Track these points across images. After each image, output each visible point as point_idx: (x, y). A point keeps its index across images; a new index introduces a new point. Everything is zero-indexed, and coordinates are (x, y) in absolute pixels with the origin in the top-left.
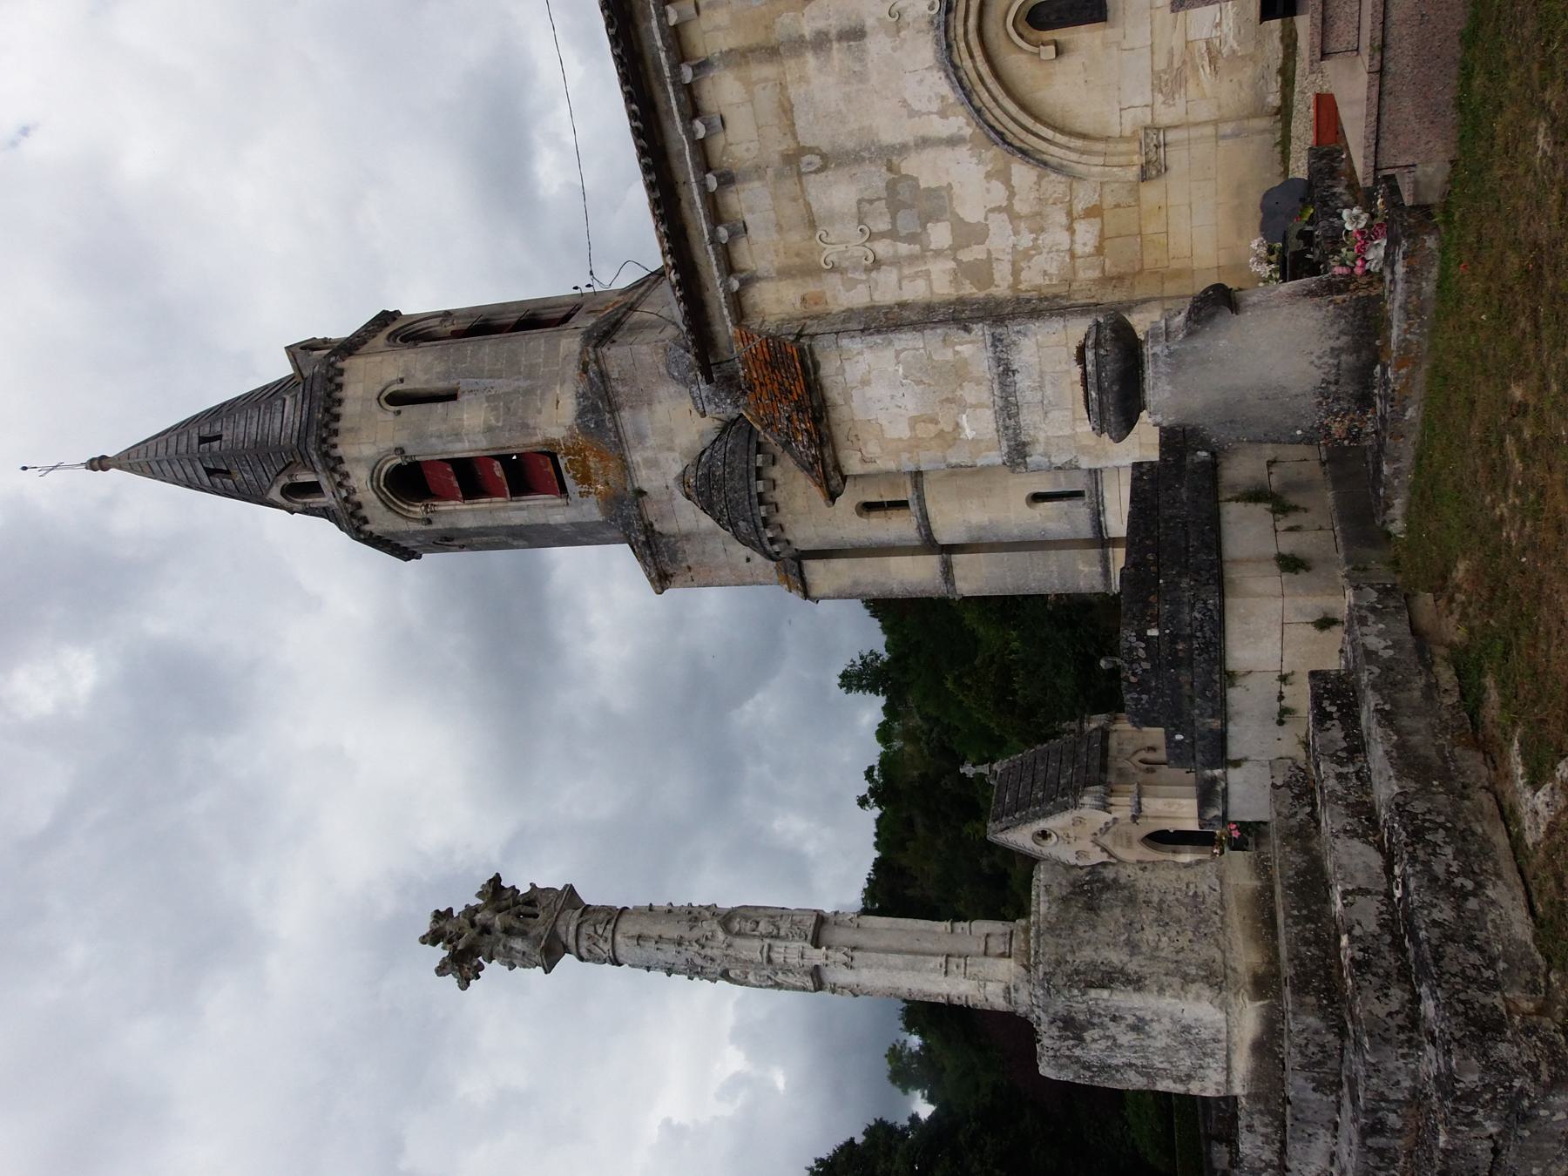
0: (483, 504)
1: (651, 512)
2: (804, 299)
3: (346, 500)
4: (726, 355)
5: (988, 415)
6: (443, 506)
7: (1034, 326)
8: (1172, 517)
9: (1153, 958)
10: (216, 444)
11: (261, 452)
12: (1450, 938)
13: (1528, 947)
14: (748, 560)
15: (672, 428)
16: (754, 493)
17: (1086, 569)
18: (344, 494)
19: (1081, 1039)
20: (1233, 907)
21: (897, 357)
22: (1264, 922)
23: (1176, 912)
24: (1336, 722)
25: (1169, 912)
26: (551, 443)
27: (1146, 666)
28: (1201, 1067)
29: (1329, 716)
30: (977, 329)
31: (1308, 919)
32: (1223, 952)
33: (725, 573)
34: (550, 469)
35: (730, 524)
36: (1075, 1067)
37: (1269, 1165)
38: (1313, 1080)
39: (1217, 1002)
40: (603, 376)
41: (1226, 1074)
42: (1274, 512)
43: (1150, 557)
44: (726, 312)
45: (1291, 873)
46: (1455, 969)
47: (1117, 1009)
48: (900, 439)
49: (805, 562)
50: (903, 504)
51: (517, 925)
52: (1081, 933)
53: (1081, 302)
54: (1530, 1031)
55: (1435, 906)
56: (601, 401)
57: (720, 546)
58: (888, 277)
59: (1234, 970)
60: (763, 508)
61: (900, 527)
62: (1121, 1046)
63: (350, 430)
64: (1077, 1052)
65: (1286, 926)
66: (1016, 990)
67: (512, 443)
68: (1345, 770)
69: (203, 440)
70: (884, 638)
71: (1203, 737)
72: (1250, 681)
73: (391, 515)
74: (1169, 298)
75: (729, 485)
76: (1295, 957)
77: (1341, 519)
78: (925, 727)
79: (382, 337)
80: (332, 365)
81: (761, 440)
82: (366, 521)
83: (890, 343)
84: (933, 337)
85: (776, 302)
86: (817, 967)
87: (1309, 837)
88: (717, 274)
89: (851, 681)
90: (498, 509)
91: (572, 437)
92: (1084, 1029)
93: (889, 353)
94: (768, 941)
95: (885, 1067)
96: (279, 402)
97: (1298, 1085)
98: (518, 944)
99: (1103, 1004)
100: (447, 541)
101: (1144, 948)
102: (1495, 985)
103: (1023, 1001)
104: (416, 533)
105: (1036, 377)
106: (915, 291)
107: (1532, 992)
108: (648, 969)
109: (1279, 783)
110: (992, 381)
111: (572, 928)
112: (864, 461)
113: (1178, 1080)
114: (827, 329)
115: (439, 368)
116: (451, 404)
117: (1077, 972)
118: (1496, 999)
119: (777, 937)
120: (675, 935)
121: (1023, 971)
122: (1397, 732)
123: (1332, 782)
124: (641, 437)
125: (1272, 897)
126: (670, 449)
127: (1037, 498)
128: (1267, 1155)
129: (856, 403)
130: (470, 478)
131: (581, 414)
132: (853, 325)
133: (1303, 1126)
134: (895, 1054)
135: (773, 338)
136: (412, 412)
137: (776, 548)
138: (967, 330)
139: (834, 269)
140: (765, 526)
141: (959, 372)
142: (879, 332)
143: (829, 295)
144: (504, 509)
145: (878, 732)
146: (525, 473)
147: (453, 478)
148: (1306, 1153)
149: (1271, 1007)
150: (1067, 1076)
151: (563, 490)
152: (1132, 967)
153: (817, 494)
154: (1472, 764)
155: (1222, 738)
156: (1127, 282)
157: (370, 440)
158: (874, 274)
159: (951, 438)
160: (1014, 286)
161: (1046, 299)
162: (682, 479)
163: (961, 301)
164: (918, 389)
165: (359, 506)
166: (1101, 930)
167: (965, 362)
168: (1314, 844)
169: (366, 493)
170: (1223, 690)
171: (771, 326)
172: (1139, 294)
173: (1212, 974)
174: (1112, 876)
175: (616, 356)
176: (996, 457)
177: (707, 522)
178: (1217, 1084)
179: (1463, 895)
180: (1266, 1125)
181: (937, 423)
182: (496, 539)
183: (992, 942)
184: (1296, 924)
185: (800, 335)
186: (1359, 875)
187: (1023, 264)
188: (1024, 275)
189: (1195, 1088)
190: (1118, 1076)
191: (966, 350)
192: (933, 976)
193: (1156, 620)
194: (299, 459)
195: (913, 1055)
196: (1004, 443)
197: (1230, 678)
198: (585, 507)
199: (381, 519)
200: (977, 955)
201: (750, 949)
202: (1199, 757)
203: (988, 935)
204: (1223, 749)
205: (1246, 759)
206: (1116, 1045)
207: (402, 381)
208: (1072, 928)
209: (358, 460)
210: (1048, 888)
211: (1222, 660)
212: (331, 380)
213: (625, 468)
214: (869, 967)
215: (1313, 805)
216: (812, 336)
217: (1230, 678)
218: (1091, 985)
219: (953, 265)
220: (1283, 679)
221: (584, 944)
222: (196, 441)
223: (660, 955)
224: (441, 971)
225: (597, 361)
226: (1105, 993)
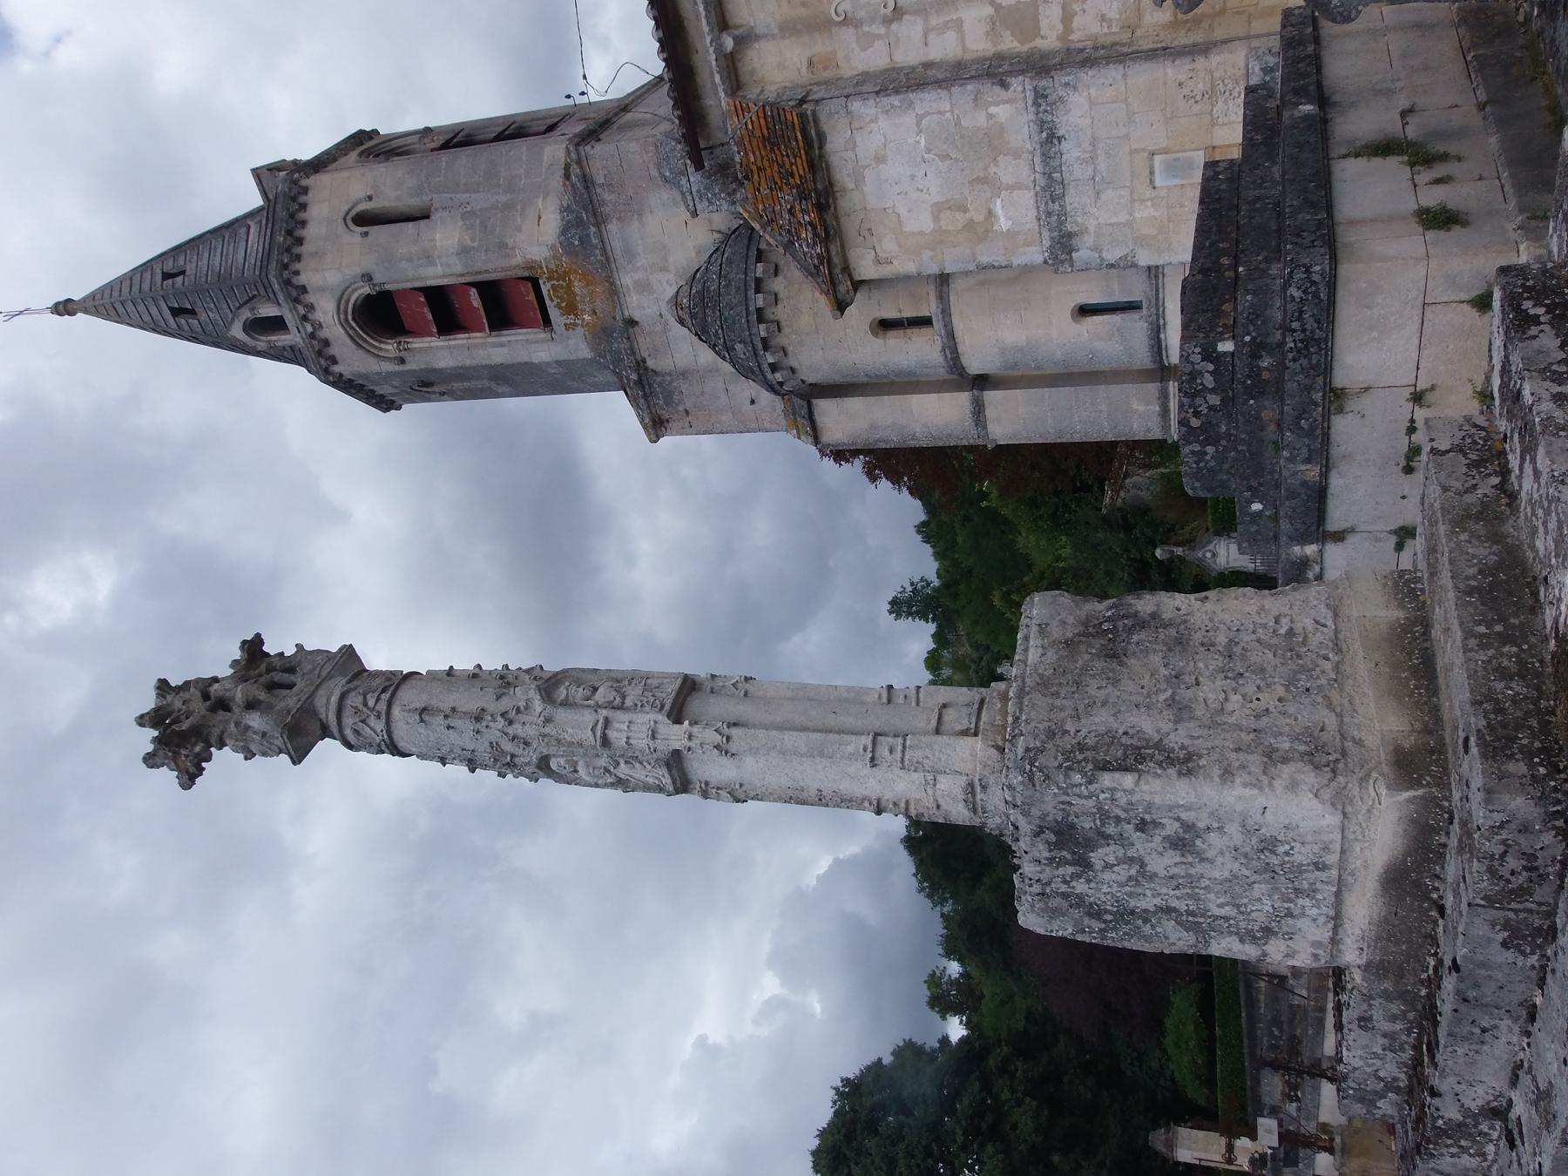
0: (460, 340)
1: (644, 346)
2: (810, 63)
3: (312, 336)
4: (720, 137)
5: (1026, 198)
6: (417, 343)
7: (1087, 76)
8: (1258, 199)
9: (1213, 725)
10: (179, 279)
11: (224, 286)
14: (753, 402)
15: (667, 238)
16: (752, 308)
17: (1141, 408)
18: (310, 329)
19: (1084, 864)
20: (1356, 648)
21: (918, 124)
22: (1414, 671)
23: (1255, 658)
24: (1547, 328)
25: (1243, 658)
26: (530, 265)
27: (1214, 400)
28: (1290, 914)
29: (1535, 320)
30: (1016, 83)
31: (1505, 639)
32: (1340, 716)
33: (726, 418)
34: (532, 297)
35: (724, 350)
36: (1076, 913)
37: (1391, 1086)
38: (1506, 926)
39: (1327, 794)
40: (587, 180)
41: (1325, 930)
42: (1412, 165)
43: (1225, 261)
44: (717, 78)
47: (1149, 807)
48: (921, 233)
49: (815, 401)
50: (925, 322)
51: (262, 696)
52: (1092, 690)
53: (1145, 47)
56: (587, 212)
57: (721, 385)
58: (911, 29)
59: (1359, 743)
60: (762, 327)
61: (919, 351)
62: (1153, 877)
63: (314, 255)
64: (1080, 887)
66: (984, 788)
67: (490, 266)
69: (167, 276)
70: (936, 565)
71: (1292, 495)
72: (1364, 403)
73: (361, 353)
74: (1258, 36)
75: (726, 307)
76: (1483, 699)
77: (1511, 163)
78: (975, 655)
79: (353, 155)
80: (295, 182)
81: (763, 246)
82: (334, 361)
83: (911, 105)
84: (962, 95)
85: (777, 66)
86: (676, 754)
87: (1501, 519)
88: (706, 29)
89: (899, 607)
90: (476, 346)
91: (554, 257)
92: (1090, 845)
93: (909, 120)
94: (604, 712)
95: (924, 993)
96: (243, 230)
97: (1470, 934)
98: (255, 720)
99: (1123, 799)
100: (427, 386)
101: (1200, 711)
103: (996, 809)
104: (391, 375)
105: (1086, 145)
106: (944, 48)
108: (443, 761)
109: (1443, 447)
110: (1033, 153)
111: (334, 700)
112: (878, 261)
113: (1248, 936)
114: (837, 93)
115: (411, 182)
116: (423, 223)
117: (1082, 747)
119: (621, 707)
120: (473, 706)
121: (994, 753)
123: (1547, 406)
124: (631, 255)
126: (664, 269)
127: (1085, 311)
128: (1391, 1069)
129: (869, 188)
130: (443, 310)
131: (565, 230)
132: (869, 87)
133: (1474, 1014)
134: (934, 980)
135: (772, 105)
136: (379, 233)
137: (779, 376)
138: (1004, 85)
139: (847, 21)
140: (765, 349)
141: (993, 142)
142: (897, 92)
143: (840, 55)
144: (484, 346)
145: (926, 660)
146: (503, 302)
147: (426, 310)
148: (1473, 1063)
149: (1430, 803)
150: (1063, 928)
151: (547, 322)
152: (1177, 739)
153: (823, 303)
155: (1320, 494)
156: (1205, 25)
157: (336, 267)
158: (894, 26)
159: (981, 230)
160: (1063, 37)
161: (1103, 47)
162: (675, 302)
163: (1000, 57)
164: (944, 166)
165: (326, 343)
166: (1127, 685)
167: (1002, 128)
168: (1508, 528)
169: (334, 331)
170: (1326, 417)
171: (771, 94)
172: (1218, 34)
173: (1320, 748)
175: (600, 154)
176: (1035, 254)
177: (706, 356)
178: (1317, 944)
180: (1393, 1018)
181: (965, 211)
182: (478, 384)
183: (950, 715)
184: (1482, 646)
185: (803, 101)
187: (1076, 7)
188: (1077, 22)
189: (1276, 954)
190: (1147, 929)
191: (1002, 112)
192: (853, 768)
193: (1232, 331)
194: (262, 292)
195: (951, 982)
196: (1046, 234)
197: (1337, 398)
198: (572, 342)
199: (352, 361)
200: (925, 733)
201: (577, 725)
202: (1285, 526)
203: (944, 706)
204: (1321, 515)
205: (1352, 530)
206: (1144, 874)
207: (370, 198)
208: (1078, 683)
209: (322, 289)
210: (1043, 629)
211: (1327, 369)
212: (294, 199)
213: (614, 292)
214: (754, 751)
215: (1505, 472)
216: (817, 102)
217: (1337, 398)
218: (1104, 767)
219: (989, 10)
220: (1418, 398)
221: (349, 721)
222: (159, 277)
223: (453, 737)
224: (150, 760)
225: (579, 162)
226: (1128, 780)
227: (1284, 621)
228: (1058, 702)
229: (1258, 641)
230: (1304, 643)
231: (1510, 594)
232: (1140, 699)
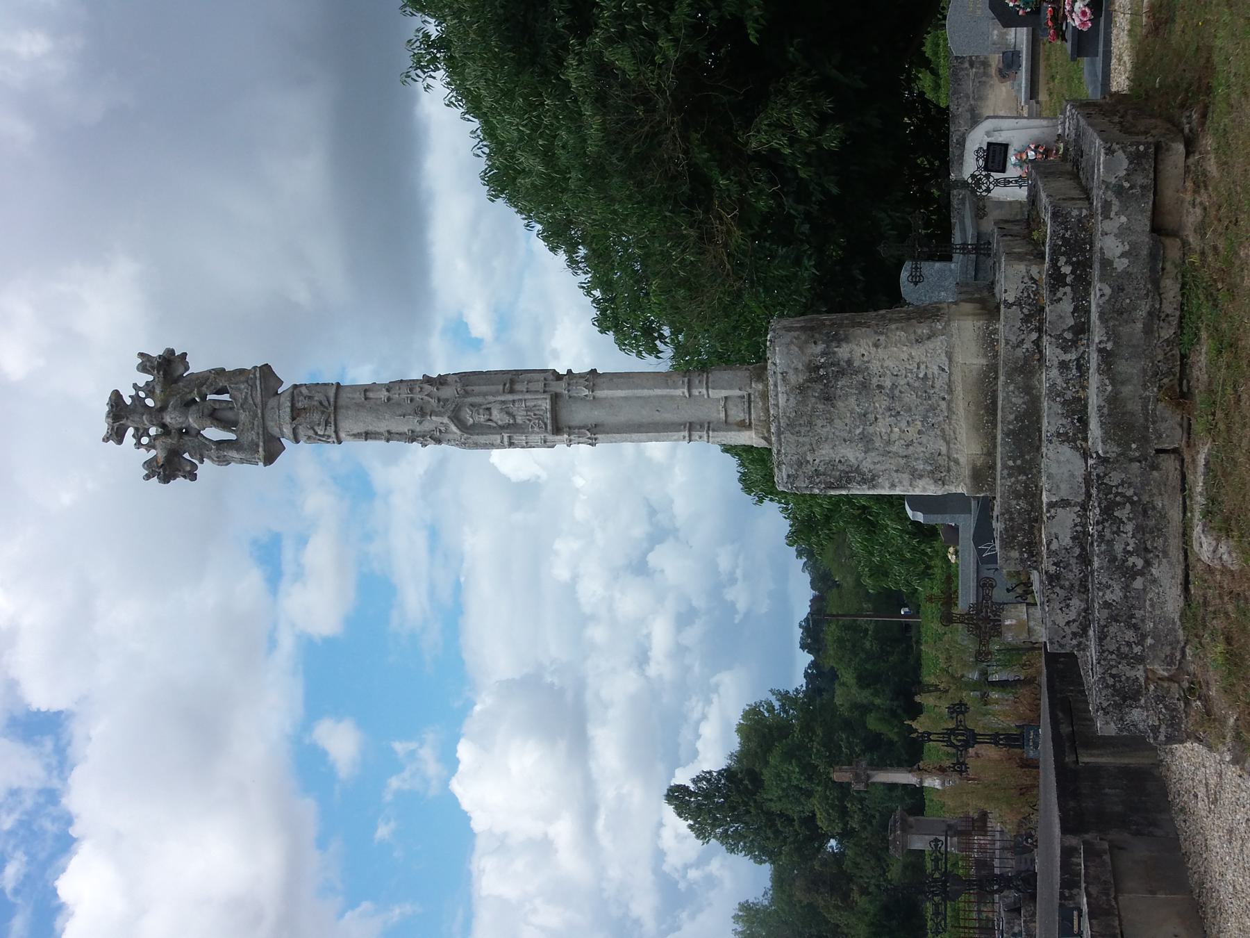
12: (1114, 619)
13: (1174, 623)
22: (987, 408)
24: (1068, 289)
25: (900, 399)
31: (1021, 470)
32: (948, 443)
45: (1012, 417)
46: (1113, 647)
54: (1160, 699)
55: (1108, 587)
59: (957, 462)
65: (1002, 478)
68: (1067, 357)
102: (1140, 659)
107: (1169, 664)
118: (1139, 673)
122: (1113, 383)
125: (996, 378)
152: (866, 466)
154: (1169, 430)
166: (838, 423)
173: (938, 468)
174: (846, 356)
179: (1132, 573)
184: (1010, 475)
186: (1063, 486)
203: (726, 398)
208: (810, 423)
227: (923, 367)
228: (801, 439)
229: (908, 384)
230: (933, 387)
231: (1029, 436)
232: (846, 435)
